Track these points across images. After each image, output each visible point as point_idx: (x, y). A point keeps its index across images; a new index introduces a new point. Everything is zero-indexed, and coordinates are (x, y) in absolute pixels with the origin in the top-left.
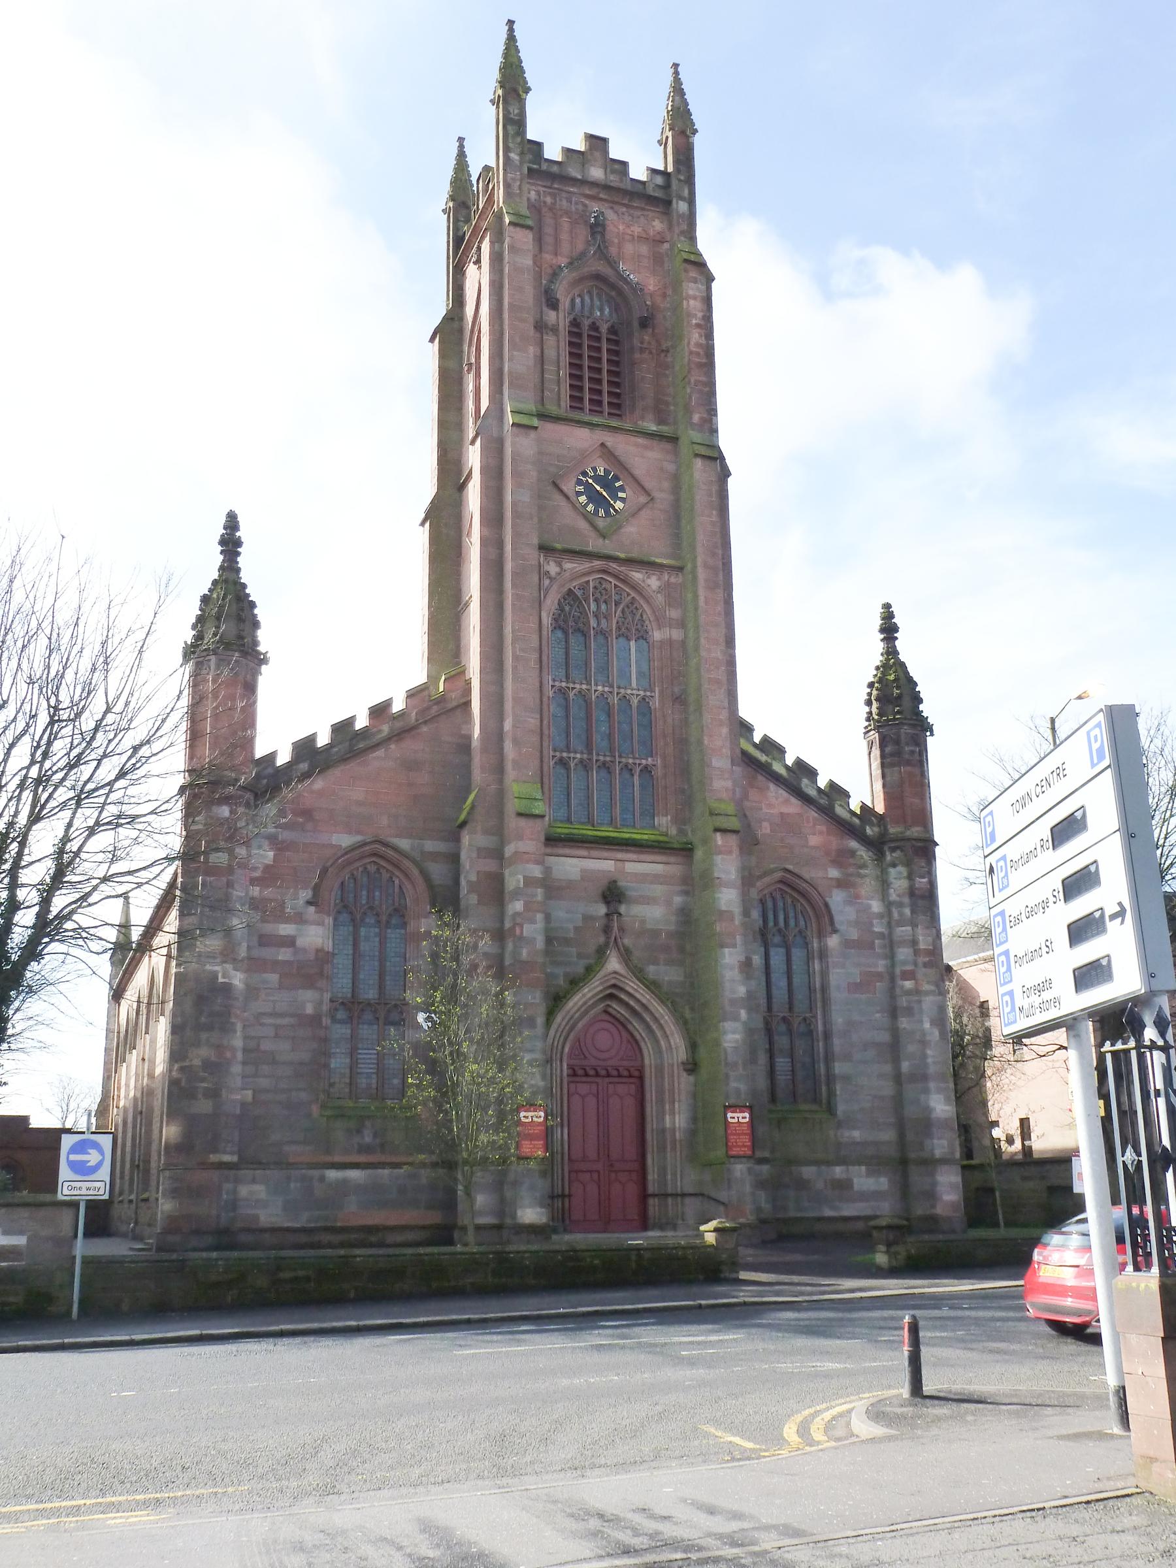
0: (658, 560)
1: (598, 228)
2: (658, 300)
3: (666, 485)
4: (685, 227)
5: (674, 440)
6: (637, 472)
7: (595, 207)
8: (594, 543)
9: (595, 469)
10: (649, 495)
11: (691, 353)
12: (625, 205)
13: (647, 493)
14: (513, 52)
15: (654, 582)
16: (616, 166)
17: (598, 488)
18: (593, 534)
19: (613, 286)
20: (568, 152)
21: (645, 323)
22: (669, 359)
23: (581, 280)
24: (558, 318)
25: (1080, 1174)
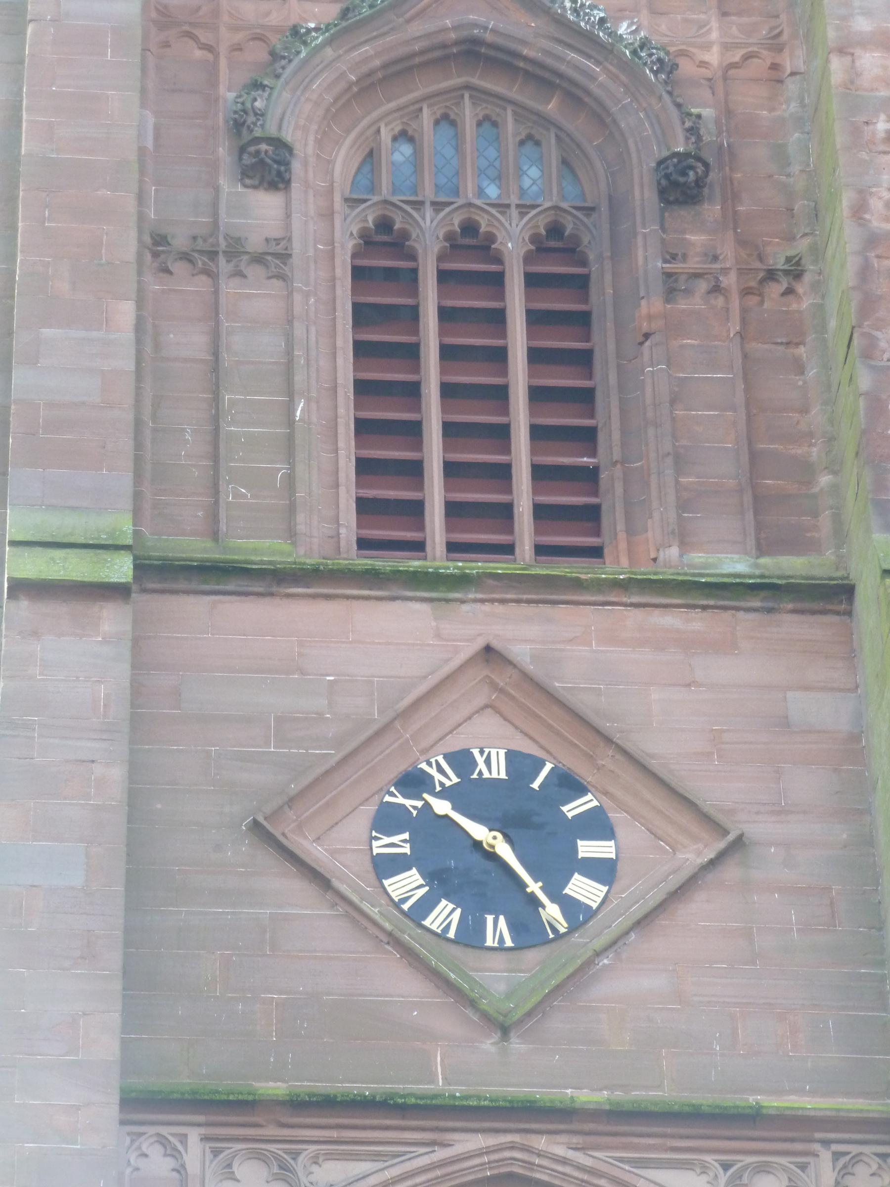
0: (772, 1103)
2: (749, 98)
3: (807, 784)
6: (658, 746)
8: (454, 1060)
9: (461, 761)
13: (711, 823)
17: (478, 831)
18: (446, 1022)
19: (543, 77)
21: (682, 185)
22: (806, 303)
23: (398, 71)
24: (312, 224)
25: (522, 347)
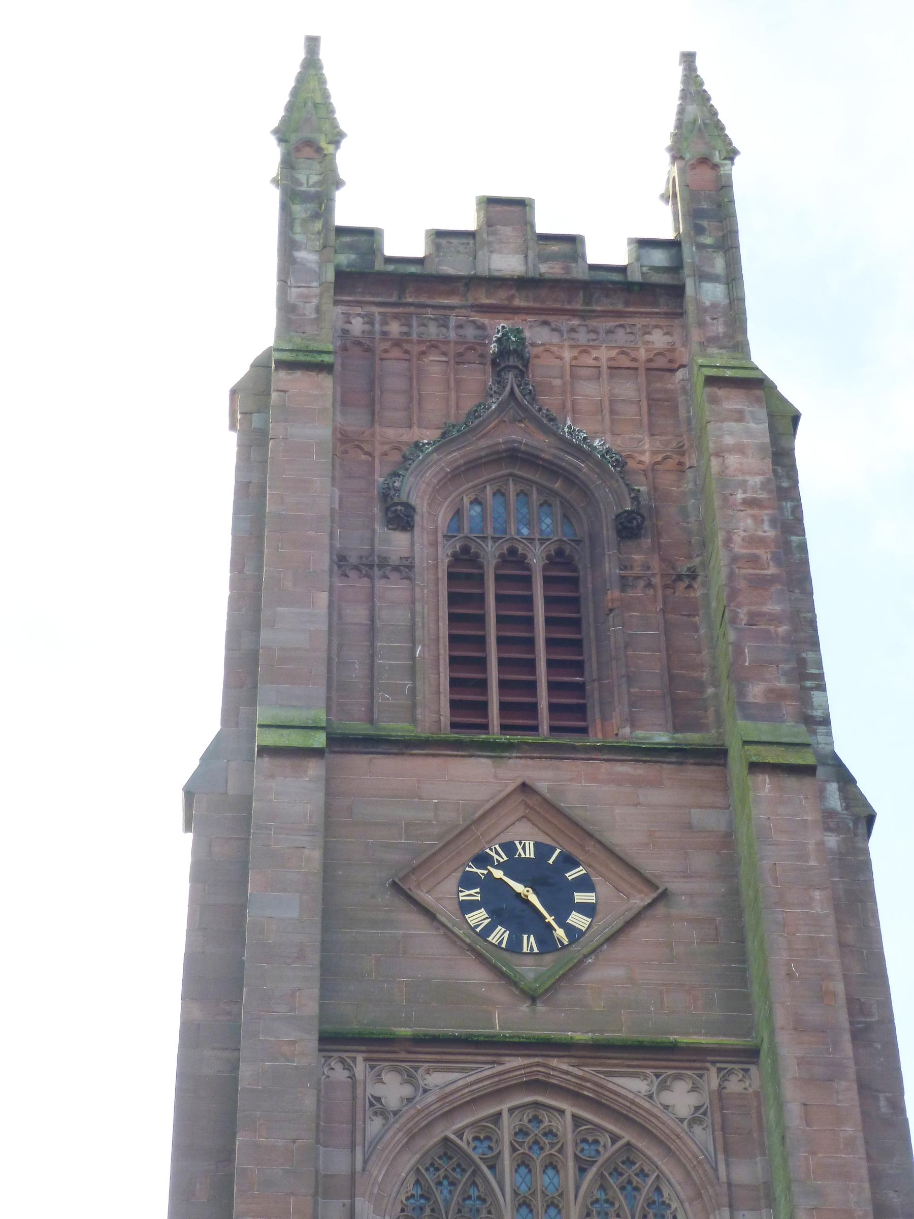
0: (683, 1040)
1: (511, 359)
2: (666, 480)
3: (702, 861)
4: (719, 328)
5: (715, 756)
7: (500, 325)
8: (505, 1016)
9: (509, 848)
10: (653, 886)
11: (735, 559)
12: (573, 313)
13: (649, 883)
14: (313, 84)
15: (681, 1098)
16: (555, 248)
17: (519, 887)
18: (501, 995)
19: (552, 469)
20: (439, 237)
21: (630, 527)
23: (473, 466)
24: (425, 547)
